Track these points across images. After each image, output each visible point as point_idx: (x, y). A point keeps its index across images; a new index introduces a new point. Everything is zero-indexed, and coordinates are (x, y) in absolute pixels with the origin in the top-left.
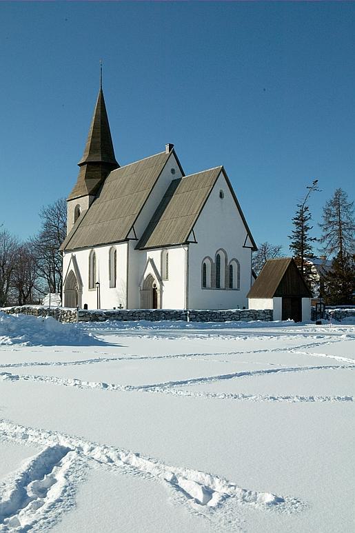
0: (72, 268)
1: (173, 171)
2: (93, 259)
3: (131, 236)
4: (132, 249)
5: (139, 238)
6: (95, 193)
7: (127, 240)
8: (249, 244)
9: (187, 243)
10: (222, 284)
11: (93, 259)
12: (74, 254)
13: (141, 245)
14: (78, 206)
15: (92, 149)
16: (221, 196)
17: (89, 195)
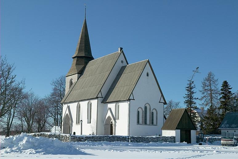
0: (67, 112)
1: (122, 62)
2: (79, 108)
3: (100, 95)
4: (100, 102)
5: (104, 96)
6: (81, 73)
7: (97, 98)
8: (162, 101)
9: (129, 100)
11: (79, 108)
12: (103, 98)
13: (105, 100)
14: (72, 79)
15: (80, 50)
16: (148, 75)
17: (78, 73)
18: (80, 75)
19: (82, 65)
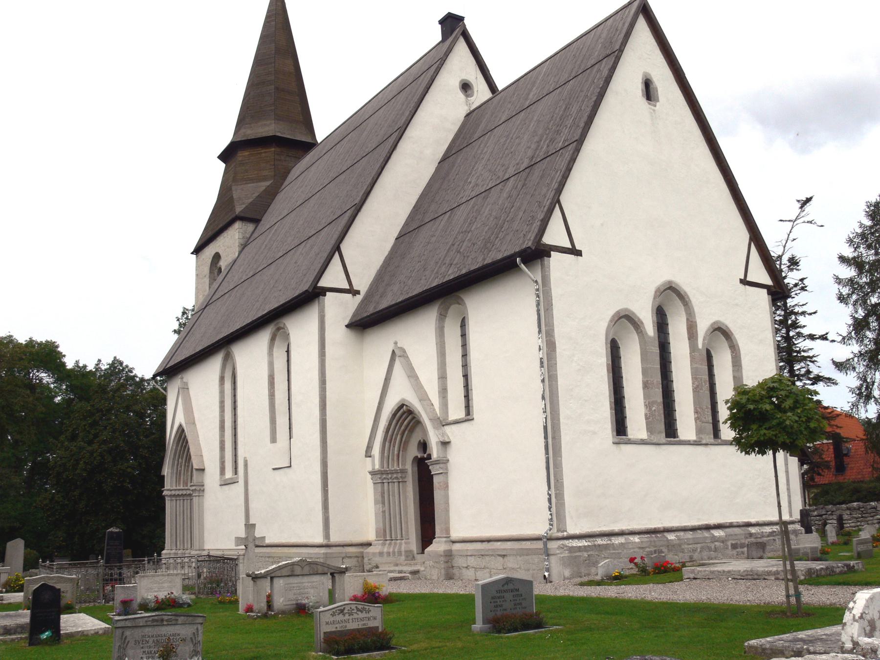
1: (466, 87)
5: (362, 283)
12: (359, 298)
14: (217, 257)
16: (649, 91)
19: (265, 179)
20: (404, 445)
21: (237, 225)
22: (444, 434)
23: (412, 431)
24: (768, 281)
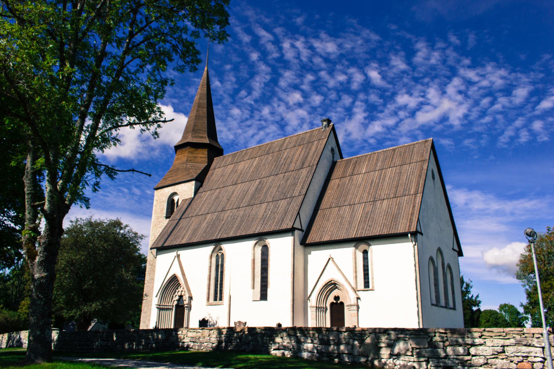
1: (332, 150)
3: (297, 225)
5: (304, 228)
6: (200, 180)
8: (456, 248)
10: (443, 302)
12: (304, 233)
18: (199, 184)
20: (327, 297)
21: (194, 182)
22: (357, 295)
23: (331, 290)
24: (457, 250)
